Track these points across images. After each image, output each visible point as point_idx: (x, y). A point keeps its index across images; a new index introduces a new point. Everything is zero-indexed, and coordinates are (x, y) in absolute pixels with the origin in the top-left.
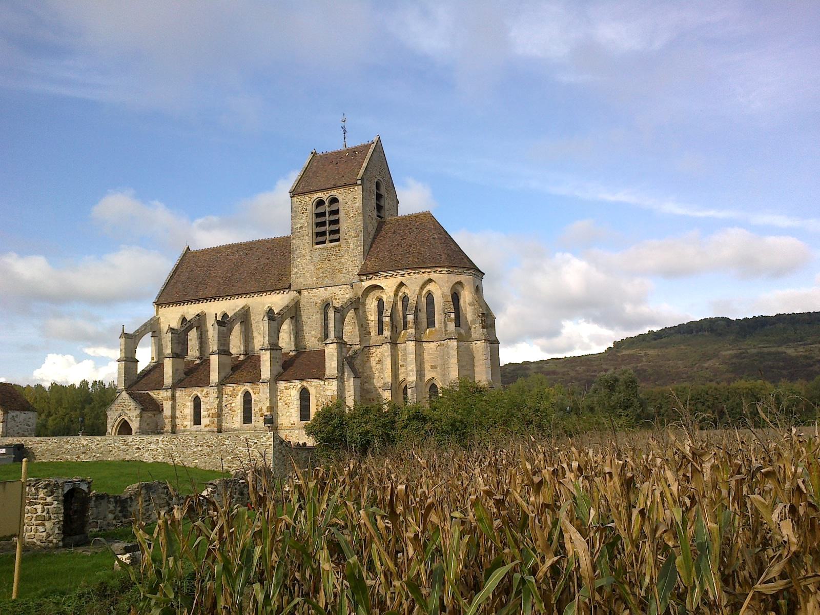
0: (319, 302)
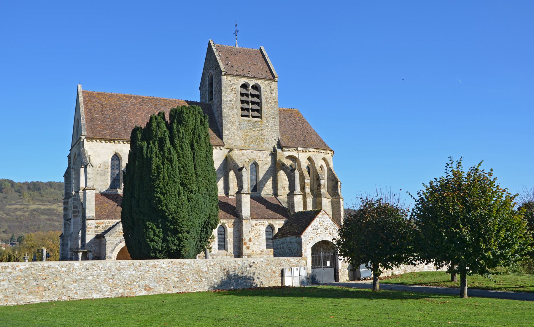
0: (248, 160)
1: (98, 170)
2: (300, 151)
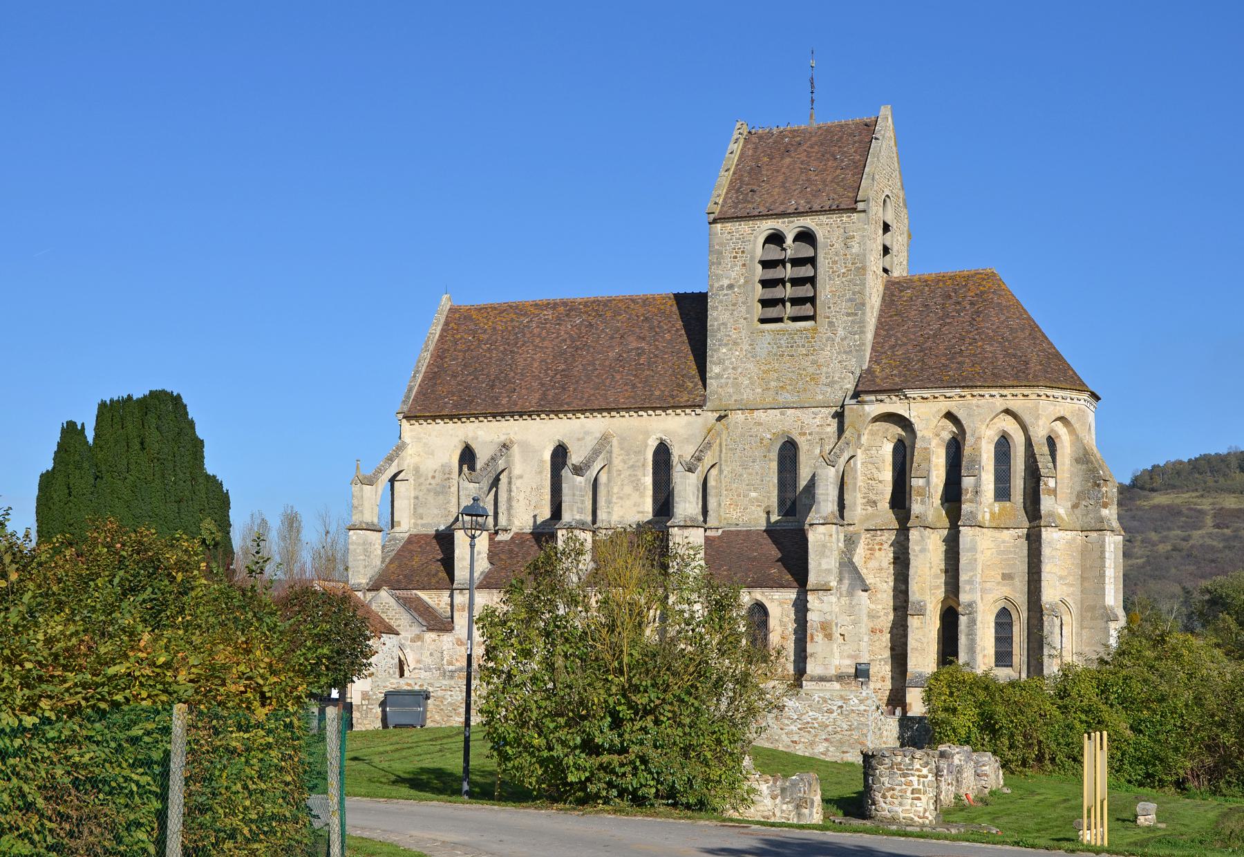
0: (769, 436)
1: (430, 484)
2: (914, 399)
